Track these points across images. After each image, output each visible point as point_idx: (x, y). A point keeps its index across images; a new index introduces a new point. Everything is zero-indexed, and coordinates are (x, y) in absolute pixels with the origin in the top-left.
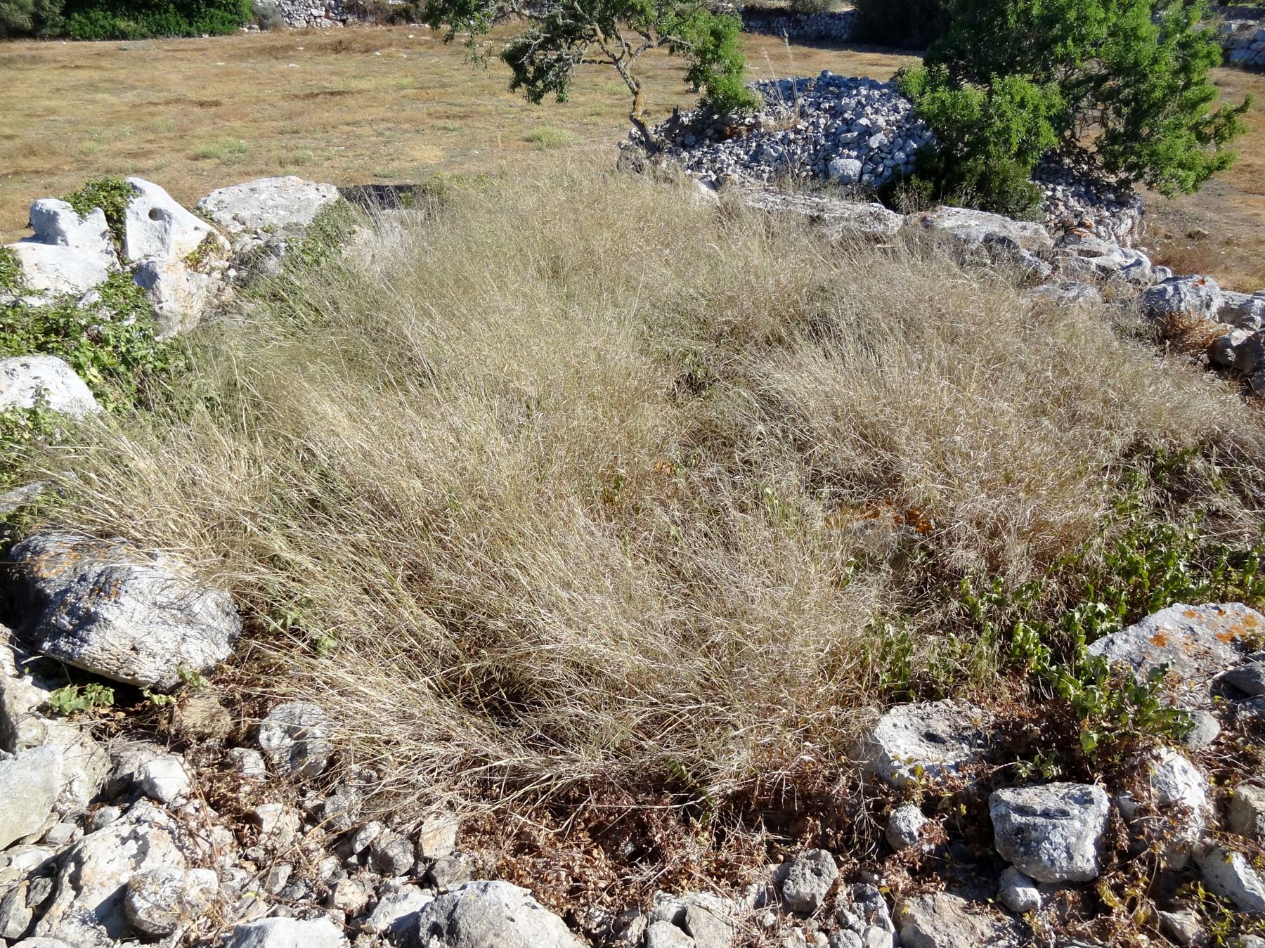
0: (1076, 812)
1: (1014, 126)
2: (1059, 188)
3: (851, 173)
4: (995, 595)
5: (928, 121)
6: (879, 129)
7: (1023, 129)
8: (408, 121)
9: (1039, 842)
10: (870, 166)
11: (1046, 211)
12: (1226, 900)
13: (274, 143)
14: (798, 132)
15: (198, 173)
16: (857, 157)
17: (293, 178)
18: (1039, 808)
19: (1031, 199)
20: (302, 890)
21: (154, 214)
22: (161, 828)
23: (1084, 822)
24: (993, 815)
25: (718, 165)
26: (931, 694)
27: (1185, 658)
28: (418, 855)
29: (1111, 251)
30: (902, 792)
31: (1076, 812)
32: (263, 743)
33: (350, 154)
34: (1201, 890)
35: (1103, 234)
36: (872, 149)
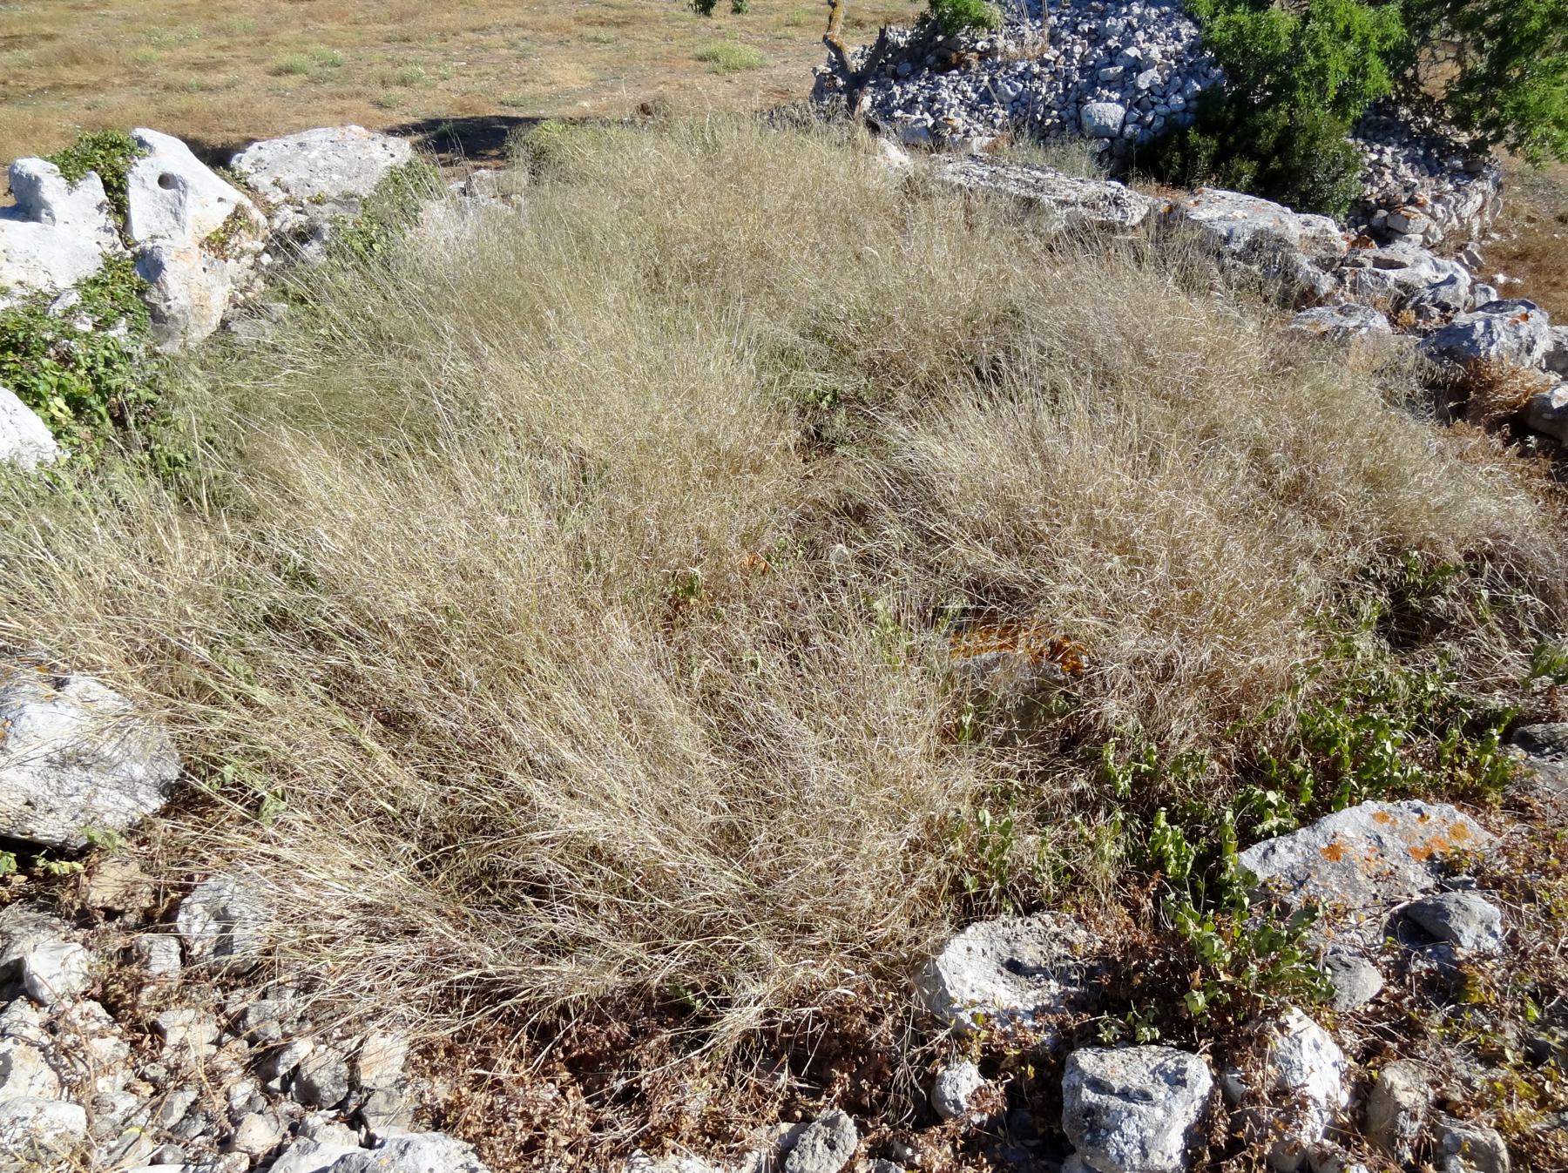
0: (1161, 1096)
1: (1332, 65)
2: (1389, 150)
3: (1110, 123)
4: (1145, 766)
5: (1219, 53)
6: (1152, 64)
7: (1345, 69)
8: (551, 27)
9: (1109, 1132)
10: (1136, 114)
11: (1365, 180)
13: (379, 54)
14: (1044, 63)
15: (277, 93)
16: (1120, 101)
17: (355, 128)
18: (1117, 1085)
19: (1347, 166)
20: (201, 1125)
21: (165, 181)
22: (31, 1044)
24: (1064, 1083)
25: (937, 106)
27: (1361, 878)
28: (353, 1084)
29: (1418, 261)
31: (1161, 1096)
32: (181, 927)
33: (473, 72)
35: (1440, 215)
36: (1140, 91)
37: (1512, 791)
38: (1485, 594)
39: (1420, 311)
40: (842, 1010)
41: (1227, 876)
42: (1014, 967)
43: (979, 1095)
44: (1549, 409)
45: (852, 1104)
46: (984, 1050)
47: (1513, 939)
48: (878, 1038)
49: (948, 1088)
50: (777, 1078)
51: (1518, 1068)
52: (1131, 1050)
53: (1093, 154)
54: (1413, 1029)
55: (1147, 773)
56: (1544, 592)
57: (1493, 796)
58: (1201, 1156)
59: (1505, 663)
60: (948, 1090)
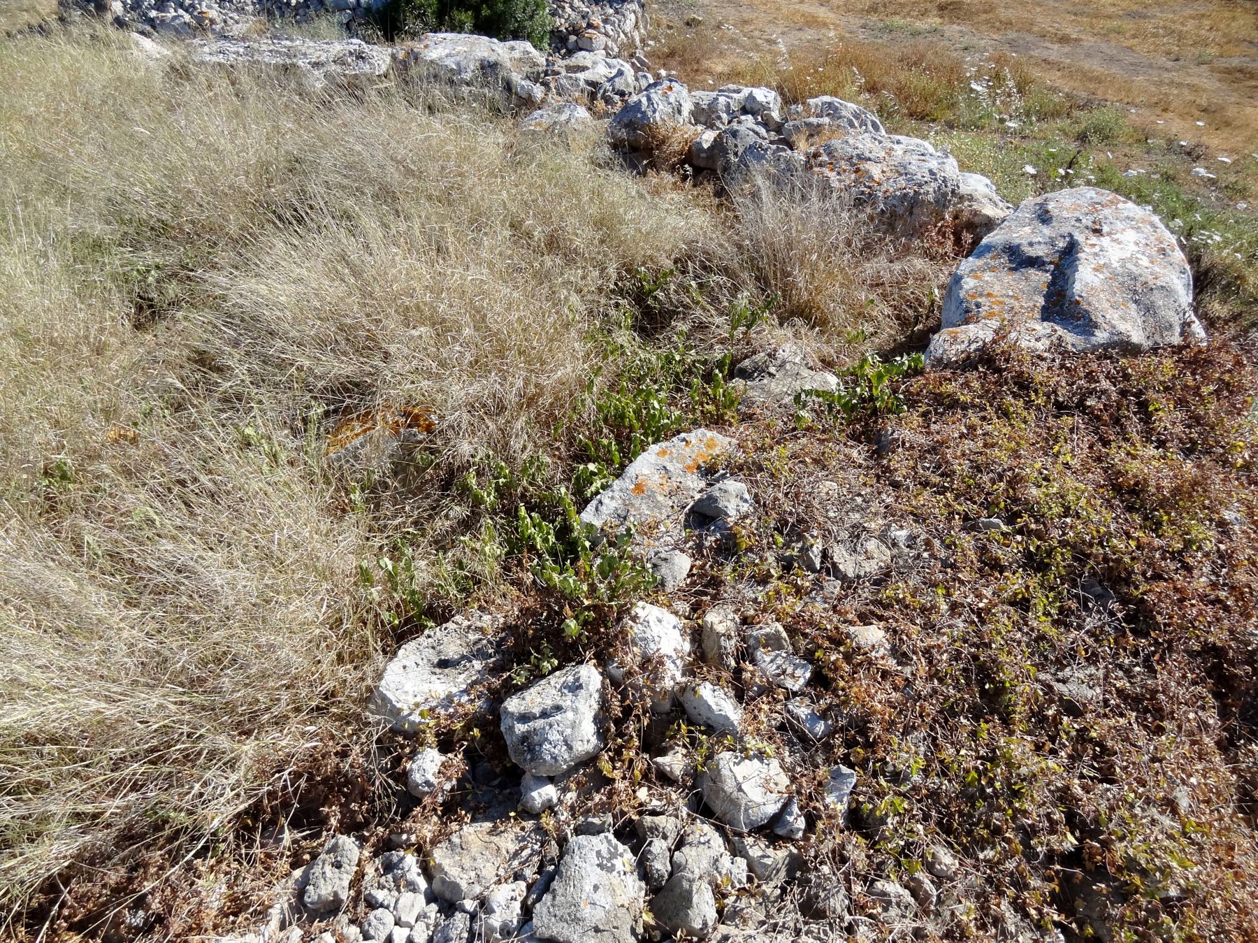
0: (569, 703)
9: (541, 745)
12: (703, 728)
18: (537, 711)
23: (575, 710)
24: (502, 729)
26: (441, 616)
27: (661, 498)
30: (415, 737)
34: (683, 727)
35: (611, 33)
37: (743, 409)
38: (693, 283)
39: (608, 101)
40: (315, 760)
41: (576, 534)
42: (444, 664)
43: (443, 771)
44: (701, 149)
45: (351, 826)
46: (437, 735)
47: (756, 498)
48: (351, 766)
49: (418, 776)
50: (280, 841)
51: (780, 578)
52: (543, 682)
53: (341, 24)
54: (716, 583)
55: (505, 484)
56: (726, 271)
57: (729, 414)
58: (608, 730)
59: (718, 327)
60: (417, 777)
